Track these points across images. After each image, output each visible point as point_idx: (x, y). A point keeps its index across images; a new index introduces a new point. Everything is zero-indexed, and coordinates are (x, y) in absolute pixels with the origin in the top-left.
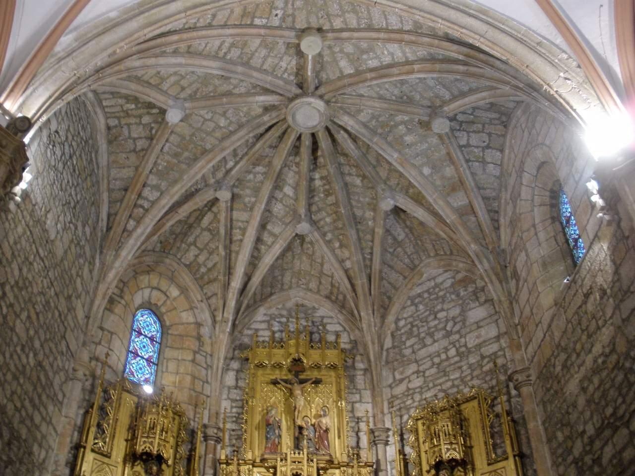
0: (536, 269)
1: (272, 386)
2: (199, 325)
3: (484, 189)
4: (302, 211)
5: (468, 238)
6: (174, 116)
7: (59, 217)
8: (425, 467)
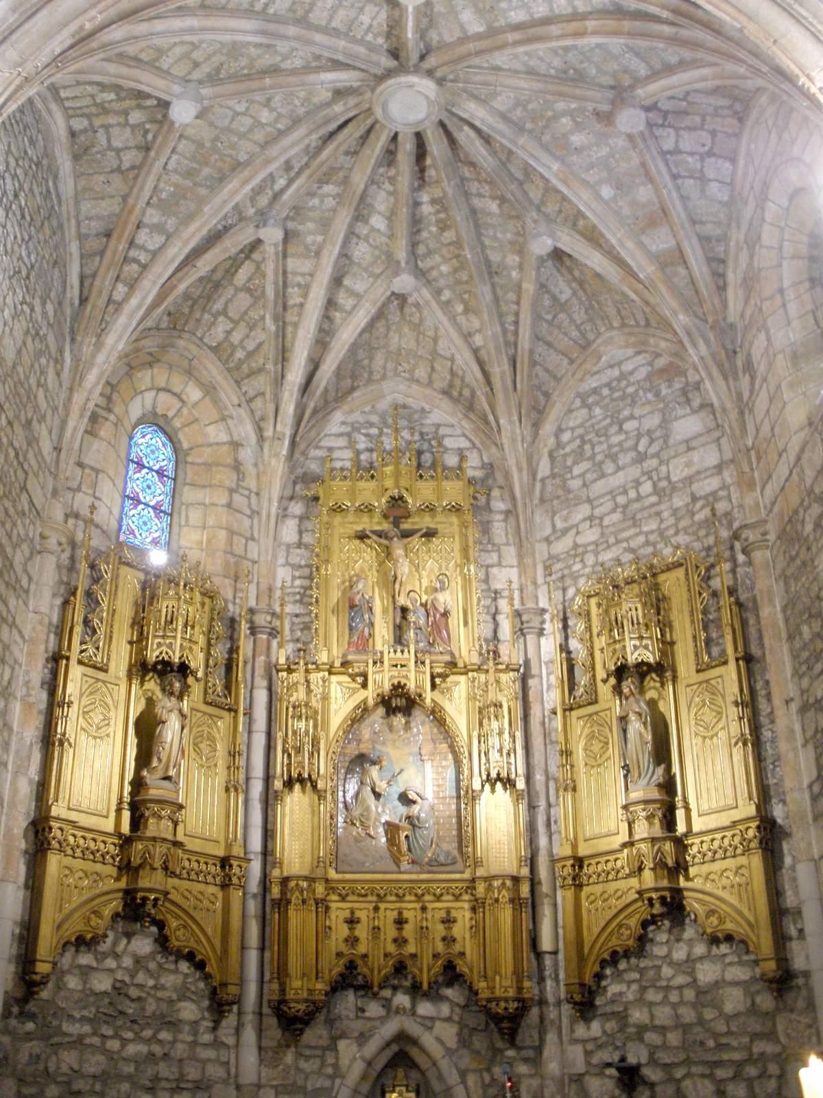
0: (781, 362)
1: (357, 542)
2: (236, 445)
3: (702, 223)
4: (402, 255)
5: (674, 304)
6: (183, 112)
7: (5, 298)
8: (600, 674)
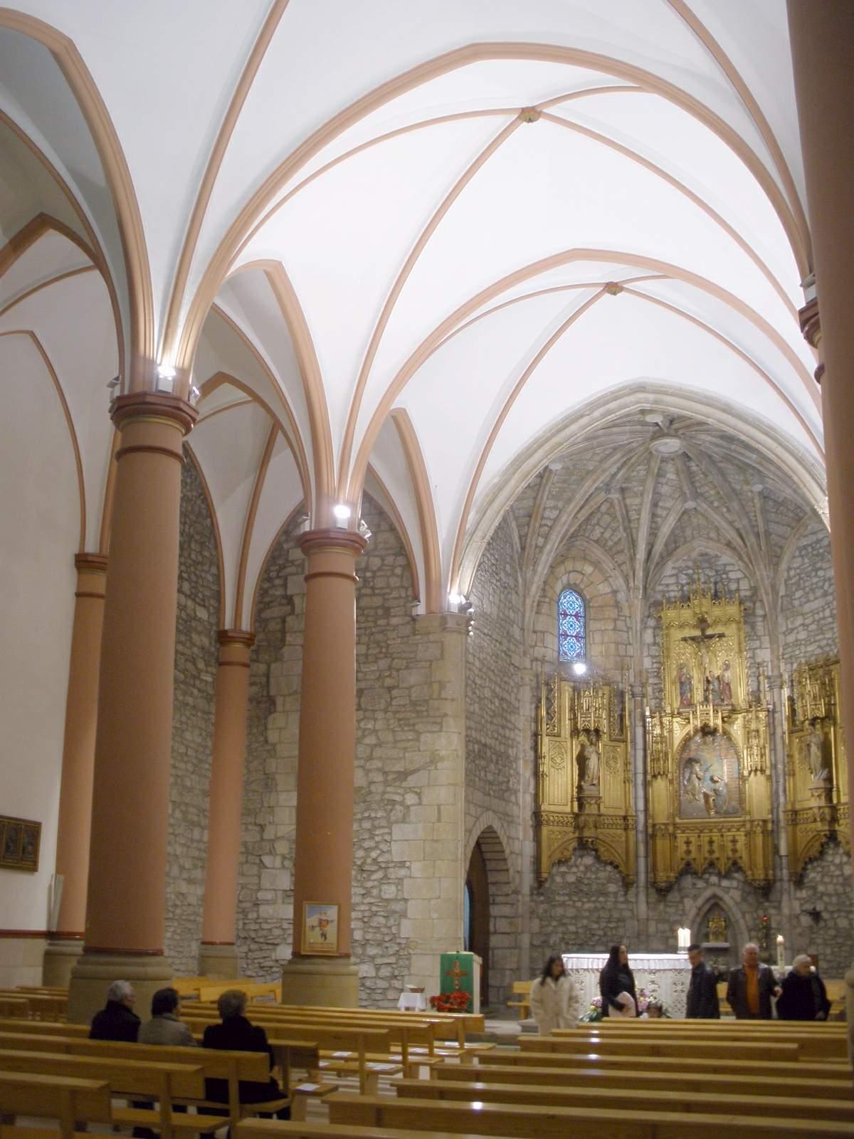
2: (615, 592)
